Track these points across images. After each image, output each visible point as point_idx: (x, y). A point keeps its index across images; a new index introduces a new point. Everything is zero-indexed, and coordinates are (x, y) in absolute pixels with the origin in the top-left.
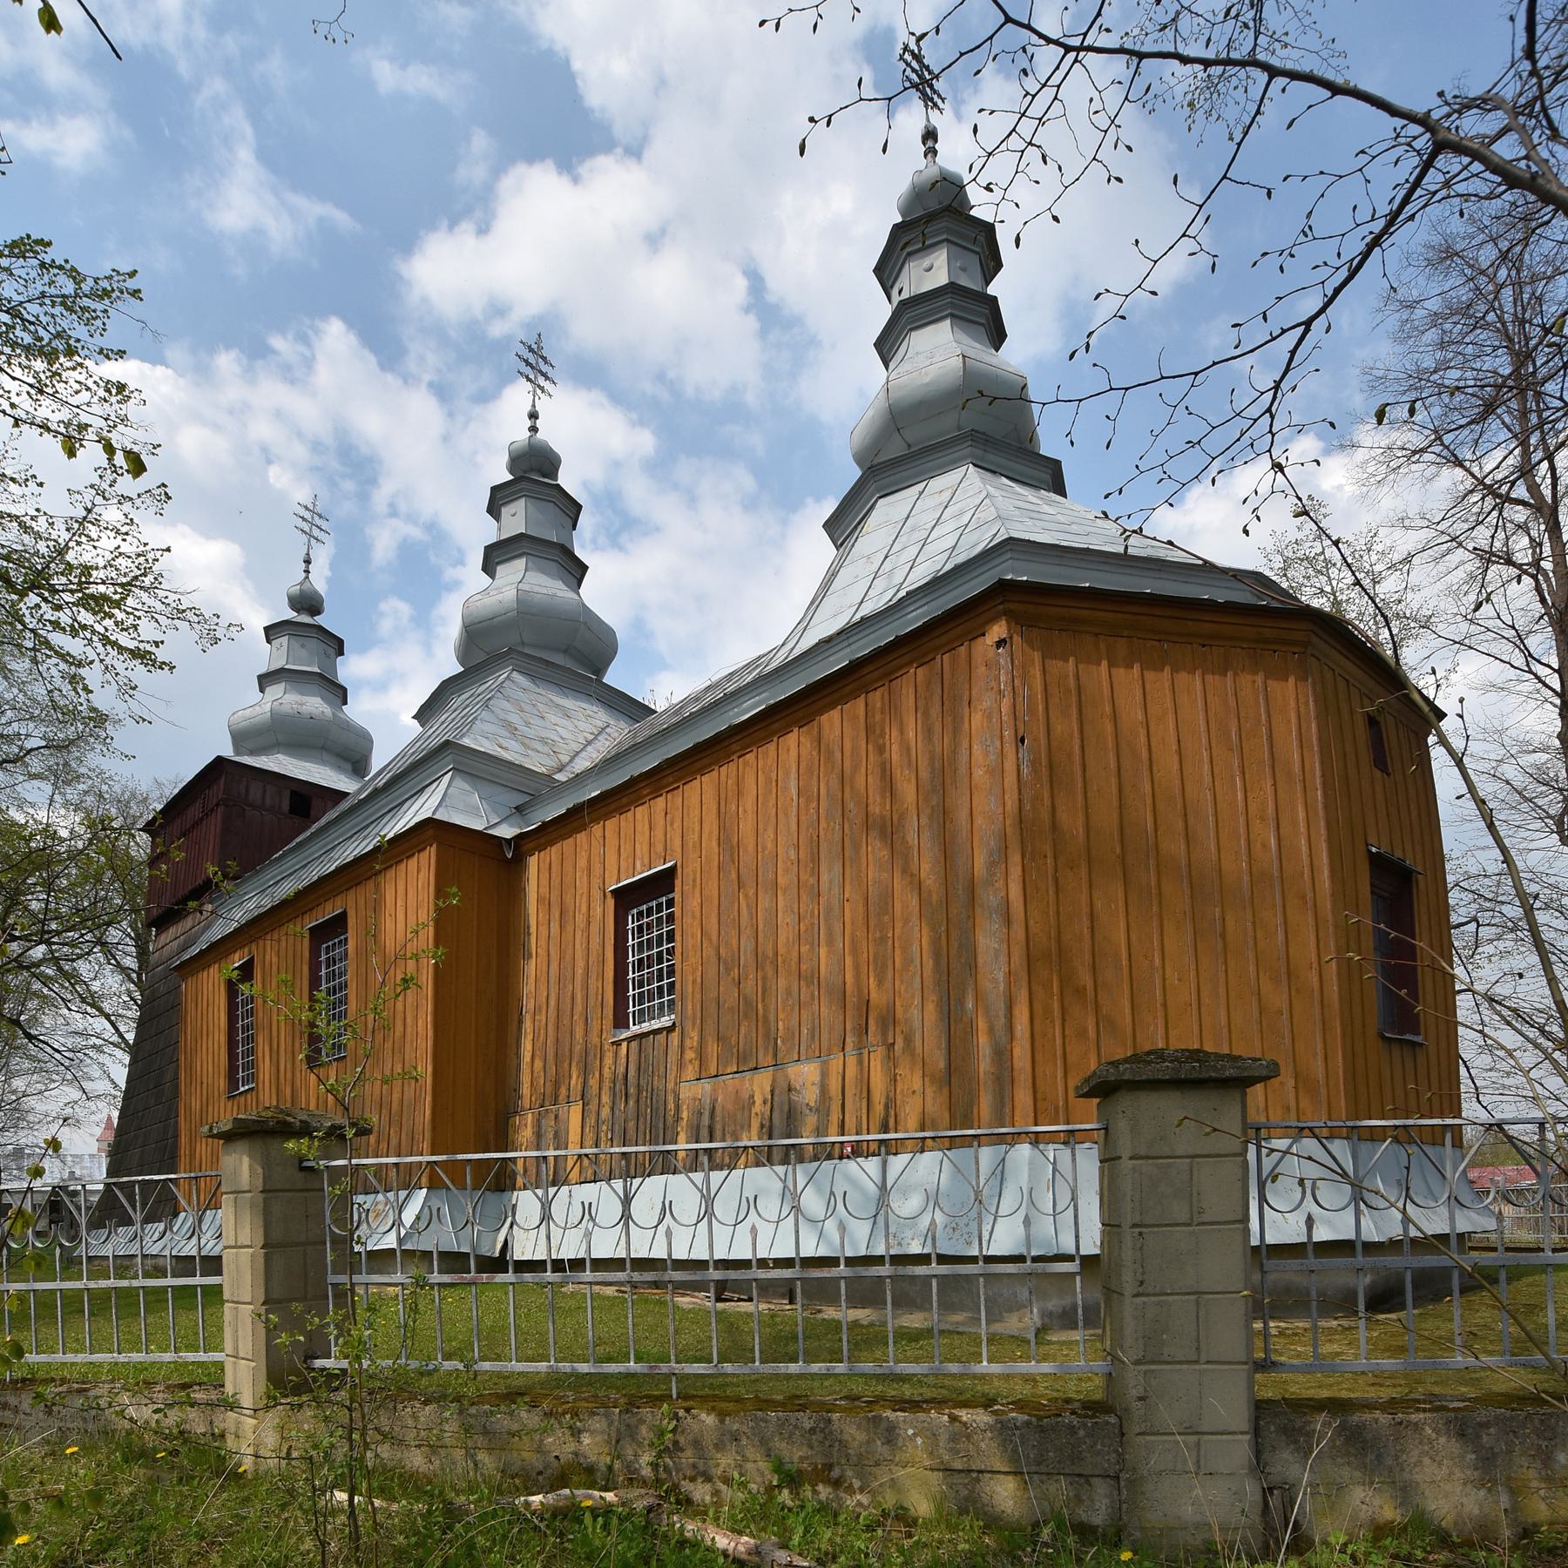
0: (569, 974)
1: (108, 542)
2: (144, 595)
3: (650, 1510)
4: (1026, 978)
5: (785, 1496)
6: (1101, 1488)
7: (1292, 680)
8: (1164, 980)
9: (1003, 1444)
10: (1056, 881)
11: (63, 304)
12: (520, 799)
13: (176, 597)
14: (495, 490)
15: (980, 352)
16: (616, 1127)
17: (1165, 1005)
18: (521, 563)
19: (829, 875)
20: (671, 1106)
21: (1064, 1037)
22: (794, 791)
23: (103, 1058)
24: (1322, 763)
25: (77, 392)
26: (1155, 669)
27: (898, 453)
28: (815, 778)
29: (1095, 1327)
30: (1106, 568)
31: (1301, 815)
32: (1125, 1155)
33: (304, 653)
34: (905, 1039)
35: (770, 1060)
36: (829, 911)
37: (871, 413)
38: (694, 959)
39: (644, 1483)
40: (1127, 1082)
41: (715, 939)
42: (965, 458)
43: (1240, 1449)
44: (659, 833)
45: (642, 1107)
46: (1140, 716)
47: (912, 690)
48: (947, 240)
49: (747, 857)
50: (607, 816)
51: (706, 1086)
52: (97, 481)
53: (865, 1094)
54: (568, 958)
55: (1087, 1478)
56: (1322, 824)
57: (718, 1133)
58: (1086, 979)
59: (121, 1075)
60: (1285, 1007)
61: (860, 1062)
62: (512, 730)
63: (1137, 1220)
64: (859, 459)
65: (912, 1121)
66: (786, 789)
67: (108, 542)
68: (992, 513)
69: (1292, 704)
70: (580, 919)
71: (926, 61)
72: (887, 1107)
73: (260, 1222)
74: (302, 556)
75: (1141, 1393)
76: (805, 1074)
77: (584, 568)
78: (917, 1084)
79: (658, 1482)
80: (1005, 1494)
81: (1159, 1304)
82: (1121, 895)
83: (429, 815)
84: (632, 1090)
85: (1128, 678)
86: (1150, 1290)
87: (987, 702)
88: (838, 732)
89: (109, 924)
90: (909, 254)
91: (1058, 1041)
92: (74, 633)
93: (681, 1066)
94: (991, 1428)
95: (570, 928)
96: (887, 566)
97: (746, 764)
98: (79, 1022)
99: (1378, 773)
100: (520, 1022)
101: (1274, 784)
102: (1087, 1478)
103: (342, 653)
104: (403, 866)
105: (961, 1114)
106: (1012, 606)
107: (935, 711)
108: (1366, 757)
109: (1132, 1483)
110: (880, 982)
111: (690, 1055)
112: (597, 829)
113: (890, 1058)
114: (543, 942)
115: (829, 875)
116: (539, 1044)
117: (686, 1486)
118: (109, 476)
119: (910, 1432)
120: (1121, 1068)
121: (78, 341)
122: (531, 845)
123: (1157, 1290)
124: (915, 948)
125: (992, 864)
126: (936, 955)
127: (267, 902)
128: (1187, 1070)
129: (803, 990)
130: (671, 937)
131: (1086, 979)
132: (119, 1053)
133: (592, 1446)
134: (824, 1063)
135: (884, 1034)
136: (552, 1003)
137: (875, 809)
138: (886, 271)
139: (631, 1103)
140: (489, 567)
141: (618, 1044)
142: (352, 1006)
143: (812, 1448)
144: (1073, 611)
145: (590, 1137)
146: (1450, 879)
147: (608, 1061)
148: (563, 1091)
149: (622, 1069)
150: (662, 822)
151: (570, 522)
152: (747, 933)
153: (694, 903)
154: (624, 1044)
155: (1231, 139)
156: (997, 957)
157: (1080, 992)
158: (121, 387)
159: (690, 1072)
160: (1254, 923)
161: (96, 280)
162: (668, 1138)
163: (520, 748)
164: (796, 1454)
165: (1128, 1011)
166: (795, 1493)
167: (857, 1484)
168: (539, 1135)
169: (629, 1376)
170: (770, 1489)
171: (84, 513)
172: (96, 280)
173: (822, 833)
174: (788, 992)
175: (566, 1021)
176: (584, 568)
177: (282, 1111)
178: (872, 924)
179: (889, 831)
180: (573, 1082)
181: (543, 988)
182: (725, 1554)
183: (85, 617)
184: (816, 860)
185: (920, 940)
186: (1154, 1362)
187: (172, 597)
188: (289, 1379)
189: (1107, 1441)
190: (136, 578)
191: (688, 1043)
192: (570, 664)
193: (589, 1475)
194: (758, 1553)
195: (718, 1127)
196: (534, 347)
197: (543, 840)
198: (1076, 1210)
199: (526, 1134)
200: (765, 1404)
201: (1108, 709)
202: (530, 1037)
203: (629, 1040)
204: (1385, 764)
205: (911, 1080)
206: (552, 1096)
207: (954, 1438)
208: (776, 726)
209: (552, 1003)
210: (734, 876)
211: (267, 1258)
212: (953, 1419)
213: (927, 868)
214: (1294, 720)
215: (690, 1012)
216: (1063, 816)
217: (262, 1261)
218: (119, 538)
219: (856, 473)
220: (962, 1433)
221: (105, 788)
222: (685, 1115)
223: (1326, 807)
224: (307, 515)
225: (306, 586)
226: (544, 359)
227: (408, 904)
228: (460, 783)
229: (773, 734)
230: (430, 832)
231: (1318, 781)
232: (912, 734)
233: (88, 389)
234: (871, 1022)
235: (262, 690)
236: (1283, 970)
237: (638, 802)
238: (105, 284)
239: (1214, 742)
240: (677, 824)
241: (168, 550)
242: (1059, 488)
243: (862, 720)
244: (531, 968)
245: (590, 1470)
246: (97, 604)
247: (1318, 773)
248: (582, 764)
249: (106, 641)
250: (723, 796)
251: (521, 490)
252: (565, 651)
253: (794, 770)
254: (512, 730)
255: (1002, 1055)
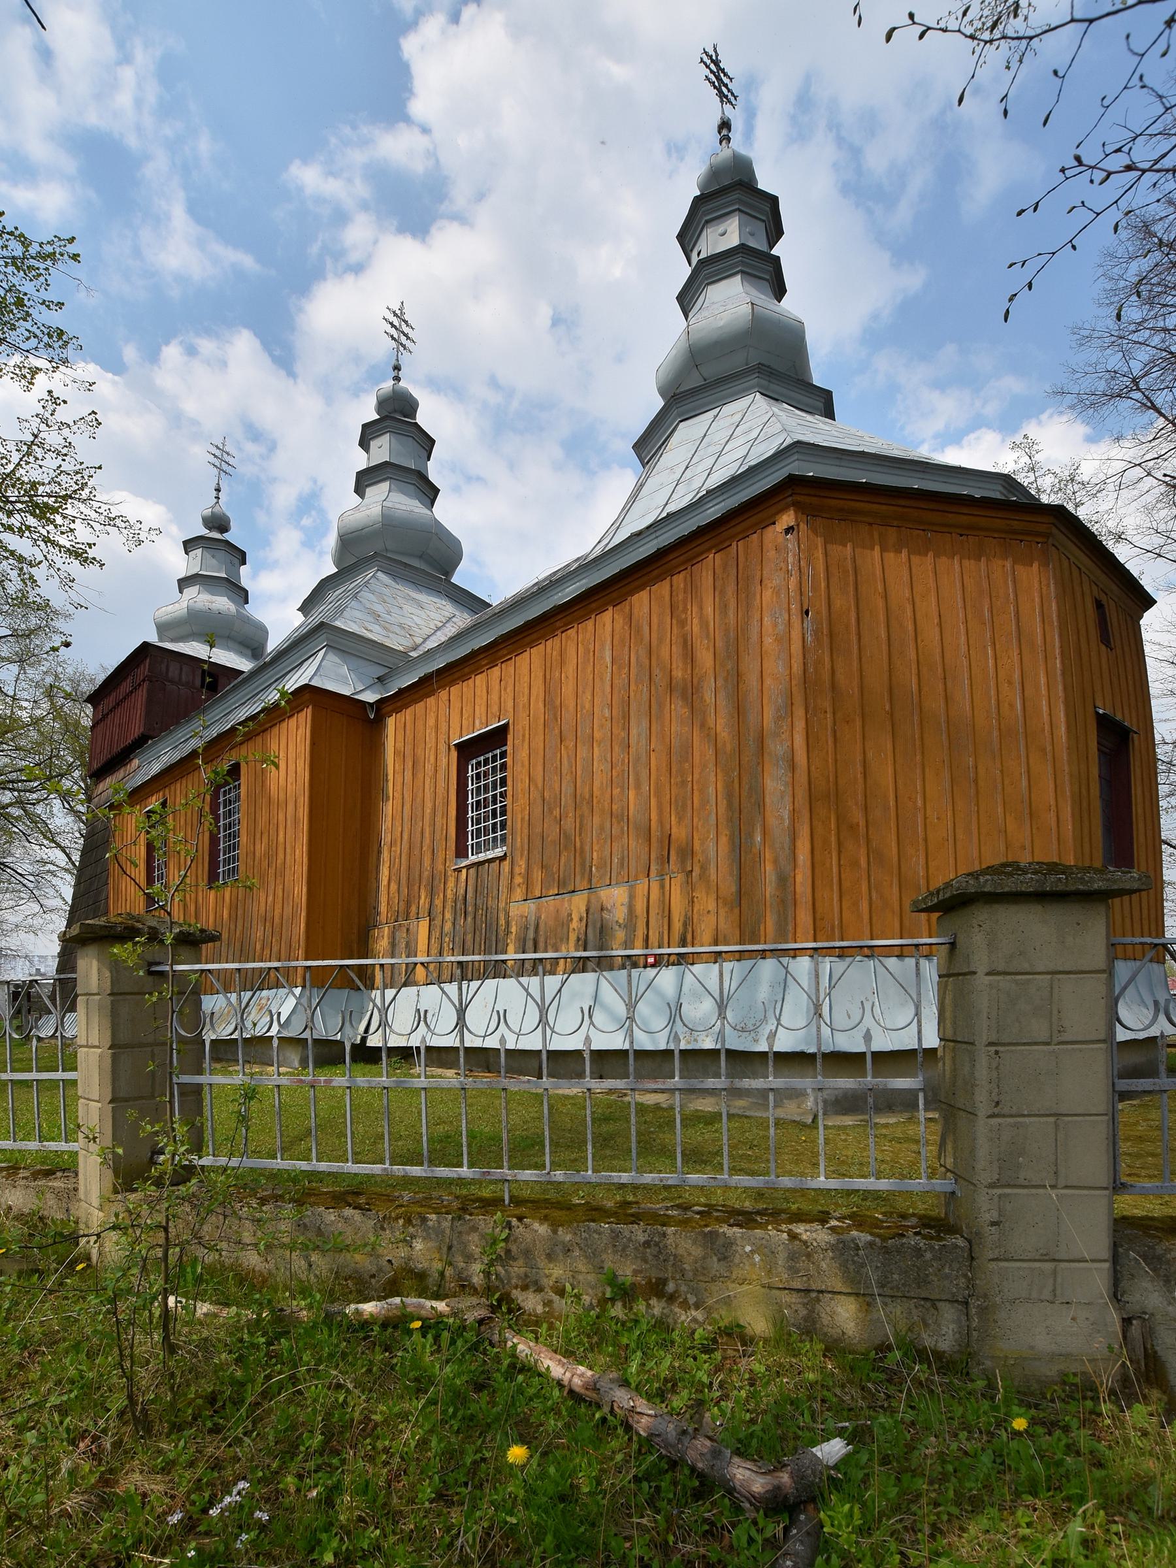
0: (419, 814)
1: (51, 462)
2: (82, 506)
3: (481, 1322)
4: (807, 815)
5: (617, 1310)
6: (949, 1316)
7: (1036, 565)
8: (925, 818)
9: (844, 1266)
10: (835, 732)
11: (14, 264)
12: (381, 671)
13: (107, 507)
14: (365, 427)
15: (765, 301)
16: (457, 939)
17: (926, 840)
18: (385, 486)
19: (638, 730)
20: (502, 922)
21: (840, 866)
22: (608, 660)
23: (55, 881)
24: (1061, 636)
25: (28, 339)
26: (920, 554)
27: (694, 387)
28: (627, 649)
29: (863, 1113)
30: (879, 469)
31: (1043, 680)
32: (981, 970)
33: (214, 561)
34: (702, 868)
35: (585, 885)
36: (638, 759)
37: (674, 352)
38: (522, 801)
39: (475, 1291)
40: (989, 894)
41: (540, 785)
42: (753, 387)
43: (1099, 1279)
44: (495, 697)
45: (478, 922)
46: (907, 594)
47: (711, 573)
48: (739, 210)
49: (568, 716)
50: (452, 683)
51: (531, 906)
52: (41, 411)
53: (666, 913)
54: (419, 800)
55: (934, 1303)
56: (1060, 687)
57: (541, 945)
58: (858, 816)
59: (68, 893)
60: (1028, 844)
61: (662, 887)
62: (377, 617)
63: (993, 1039)
64: (662, 392)
65: (707, 936)
66: (603, 658)
67: (51, 462)
68: (778, 427)
69: (1036, 585)
70: (429, 768)
71: (722, 65)
72: (685, 925)
73: (107, 1024)
74: (214, 486)
75: (995, 1216)
76: (616, 897)
77: (436, 491)
78: (712, 906)
79: (489, 1290)
80: (844, 1315)
81: (1016, 1126)
82: (889, 746)
83: (306, 682)
84: (470, 909)
85: (897, 561)
86: (1006, 1111)
87: (775, 580)
88: (646, 610)
89: (62, 776)
90: (707, 222)
91: (835, 869)
92: (21, 532)
93: (511, 889)
94: (833, 1248)
95: (420, 776)
96: (688, 474)
97: (568, 638)
98: (43, 853)
99: (1103, 647)
100: (379, 852)
101: (1020, 654)
102: (934, 1303)
103: (244, 563)
104: (284, 725)
105: (748, 932)
106: (799, 498)
107: (731, 589)
108: (1094, 633)
109: (983, 1311)
110: (680, 819)
111: (518, 880)
112: (443, 694)
113: (689, 885)
114: (399, 787)
115: (638, 730)
116: (394, 871)
117: (515, 1293)
118: (50, 407)
119: (748, 1249)
120: (982, 879)
121: (25, 294)
122: (389, 708)
123: (1014, 1111)
124: (711, 790)
125: (778, 719)
126: (729, 796)
127: (177, 756)
128: (1051, 883)
129: (615, 826)
130: (503, 782)
131: (858, 816)
132: (68, 877)
133: (421, 1252)
134: (631, 886)
135: (683, 862)
136: (406, 836)
137: (678, 674)
138: (687, 237)
139: (469, 919)
140: (360, 490)
141: (459, 870)
142: (243, 839)
143: (646, 1261)
144: (852, 504)
145: (434, 951)
146: (1158, 737)
147: (451, 884)
148: (414, 909)
149: (462, 891)
150: (497, 687)
151: (426, 454)
152: (567, 778)
153: (523, 754)
154: (464, 871)
155: (1008, 68)
156: (782, 798)
157: (853, 828)
158: (61, 333)
159: (519, 894)
160: (1002, 771)
161: (41, 244)
162: (500, 948)
163: (384, 633)
164: (627, 1272)
165: (894, 844)
166: (628, 1306)
167: (692, 1300)
168: (393, 944)
169: (461, 1182)
170: (603, 1302)
171: (32, 438)
172: (41, 244)
173: (632, 694)
174: (602, 828)
175: (417, 852)
176: (436, 491)
177: (133, 917)
178: (673, 770)
179: (690, 693)
180: (422, 902)
181: (398, 823)
182: (560, 1384)
183: (31, 521)
184: (627, 717)
185: (713, 786)
186: (1009, 1186)
187: (104, 507)
188: (128, 1174)
189: (956, 1266)
190: (75, 492)
191: (517, 870)
192: (423, 566)
193: (415, 1280)
194: (596, 1389)
195: (541, 940)
196: (398, 312)
197: (399, 704)
198: (919, 1022)
199: (383, 944)
200: (595, 1212)
201: (880, 588)
202: (387, 865)
203: (468, 867)
204: (1109, 642)
205: (706, 902)
206: (405, 913)
207: (792, 1257)
208: (594, 605)
209: (406, 836)
210: (557, 731)
211: (114, 1058)
212: (793, 1236)
213: (722, 725)
214: (1037, 600)
215: (519, 844)
216: (840, 677)
217: (109, 1061)
218: (60, 458)
219: (660, 403)
220: (801, 1252)
221: (60, 669)
222: (513, 929)
223: (1063, 674)
224: (218, 453)
225: (217, 509)
226: (406, 322)
227: (290, 753)
228: (333, 658)
229: (592, 612)
230: (307, 696)
231: (1057, 651)
232: (710, 610)
233: (36, 336)
234: (672, 853)
235: (181, 592)
236: (1027, 811)
237: (477, 671)
238: (49, 249)
239: (969, 617)
240: (510, 689)
241: (100, 468)
242: (829, 414)
243: (667, 598)
244: (388, 809)
245: (421, 1276)
246: (43, 512)
247: (1057, 644)
248: (431, 644)
249: (47, 540)
250: (548, 665)
251: (386, 427)
252: (420, 557)
253: (609, 642)
254: (377, 617)
255: (784, 881)
